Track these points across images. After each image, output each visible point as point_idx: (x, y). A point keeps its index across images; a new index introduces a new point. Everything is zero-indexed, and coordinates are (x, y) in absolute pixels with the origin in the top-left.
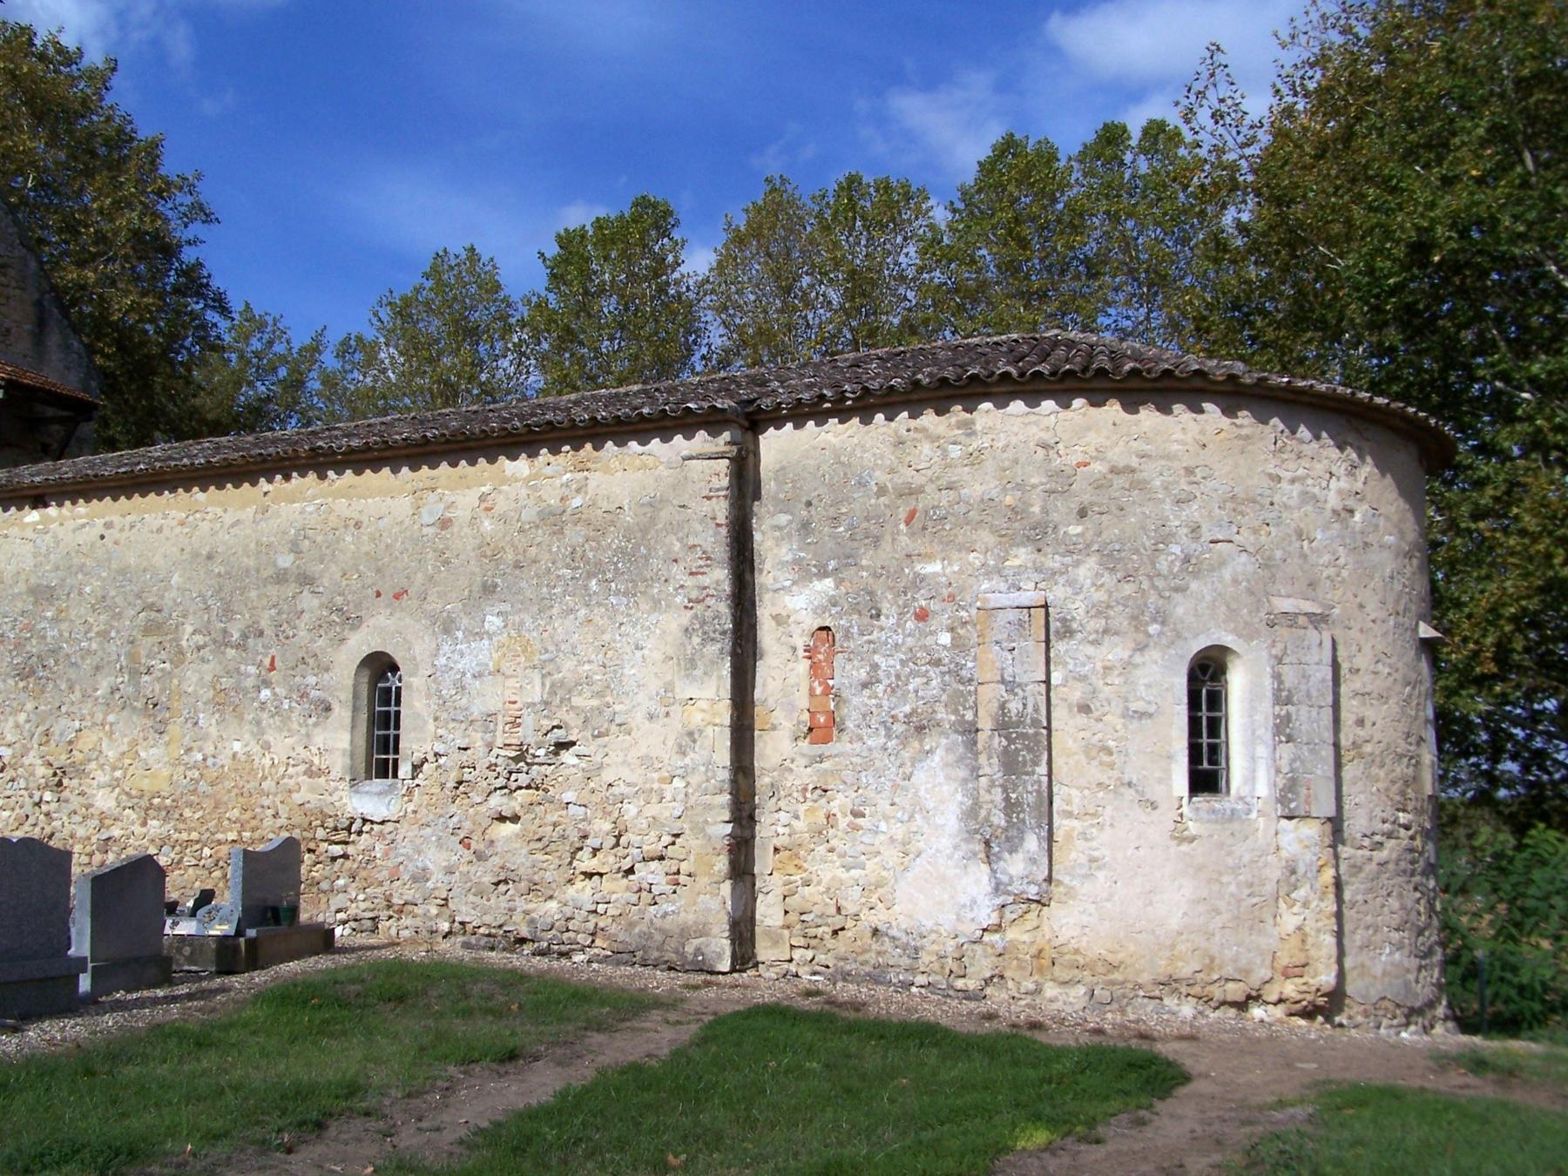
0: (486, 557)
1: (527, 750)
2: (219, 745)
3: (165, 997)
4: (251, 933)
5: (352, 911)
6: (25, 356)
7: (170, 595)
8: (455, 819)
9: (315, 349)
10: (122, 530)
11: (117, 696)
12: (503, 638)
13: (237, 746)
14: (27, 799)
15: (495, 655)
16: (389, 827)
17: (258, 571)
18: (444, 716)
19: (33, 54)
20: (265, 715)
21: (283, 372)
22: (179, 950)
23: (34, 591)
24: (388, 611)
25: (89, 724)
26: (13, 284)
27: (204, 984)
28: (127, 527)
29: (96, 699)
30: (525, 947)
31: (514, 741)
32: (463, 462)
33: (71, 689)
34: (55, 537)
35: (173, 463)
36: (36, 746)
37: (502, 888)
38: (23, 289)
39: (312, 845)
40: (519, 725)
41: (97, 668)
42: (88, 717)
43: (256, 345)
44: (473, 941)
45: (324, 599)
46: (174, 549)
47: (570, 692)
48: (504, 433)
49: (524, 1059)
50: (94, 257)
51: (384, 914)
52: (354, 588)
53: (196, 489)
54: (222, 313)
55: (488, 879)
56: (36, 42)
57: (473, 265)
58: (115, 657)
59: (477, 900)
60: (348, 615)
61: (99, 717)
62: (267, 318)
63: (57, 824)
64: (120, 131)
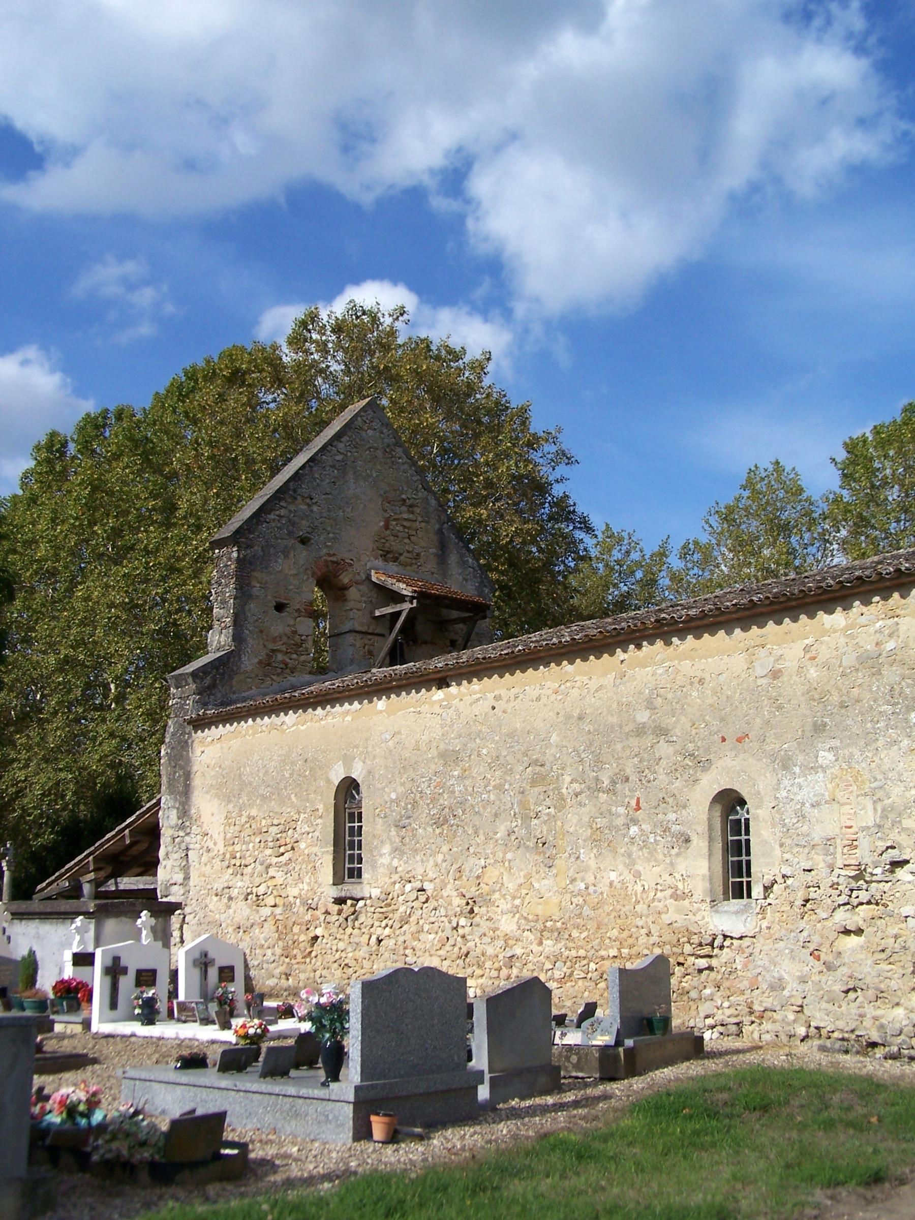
0: (814, 700)
1: (865, 870)
2: (598, 875)
3: (554, 1105)
4: (629, 1043)
5: (719, 1017)
6: (433, 573)
7: (550, 752)
8: (805, 934)
9: (662, 554)
10: (508, 701)
11: (513, 838)
12: (836, 770)
13: (613, 876)
14: (447, 924)
15: (829, 786)
16: (746, 942)
17: (621, 727)
18: (788, 842)
19: (431, 357)
20: (635, 848)
21: (639, 575)
22: (568, 1058)
23: (443, 755)
24: (733, 753)
25: (492, 861)
26: (420, 519)
27: (589, 1091)
28: (512, 698)
29: (496, 841)
30: (876, 1050)
31: (853, 862)
32: (787, 620)
33: (476, 833)
34: (457, 710)
35: (545, 643)
36: (452, 881)
37: (852, 995)
38: (428, 522)
39: (681, 960)
40: (856, 847)
41: (496, 815)
42: (491, 856)
43: (617, 555)
44: (829, 1045)
45: (678, 747)
46: (551, 714)
47: (900, 815)
48: (819, 592)
49: (891, 1183)
50: (486, 497)
51: (747, 1020)
52: (702, 736)
53: (565, 663)
54: (587, 532)
55: (838, 988)
56: (432, 348)
57: (779, 476)
58: (510, 805)
59: (829, 1006)
60: (699, 759)
61: (500, 855)
62: (623, 534)
63: (471, 944)
64: (497, 403)
